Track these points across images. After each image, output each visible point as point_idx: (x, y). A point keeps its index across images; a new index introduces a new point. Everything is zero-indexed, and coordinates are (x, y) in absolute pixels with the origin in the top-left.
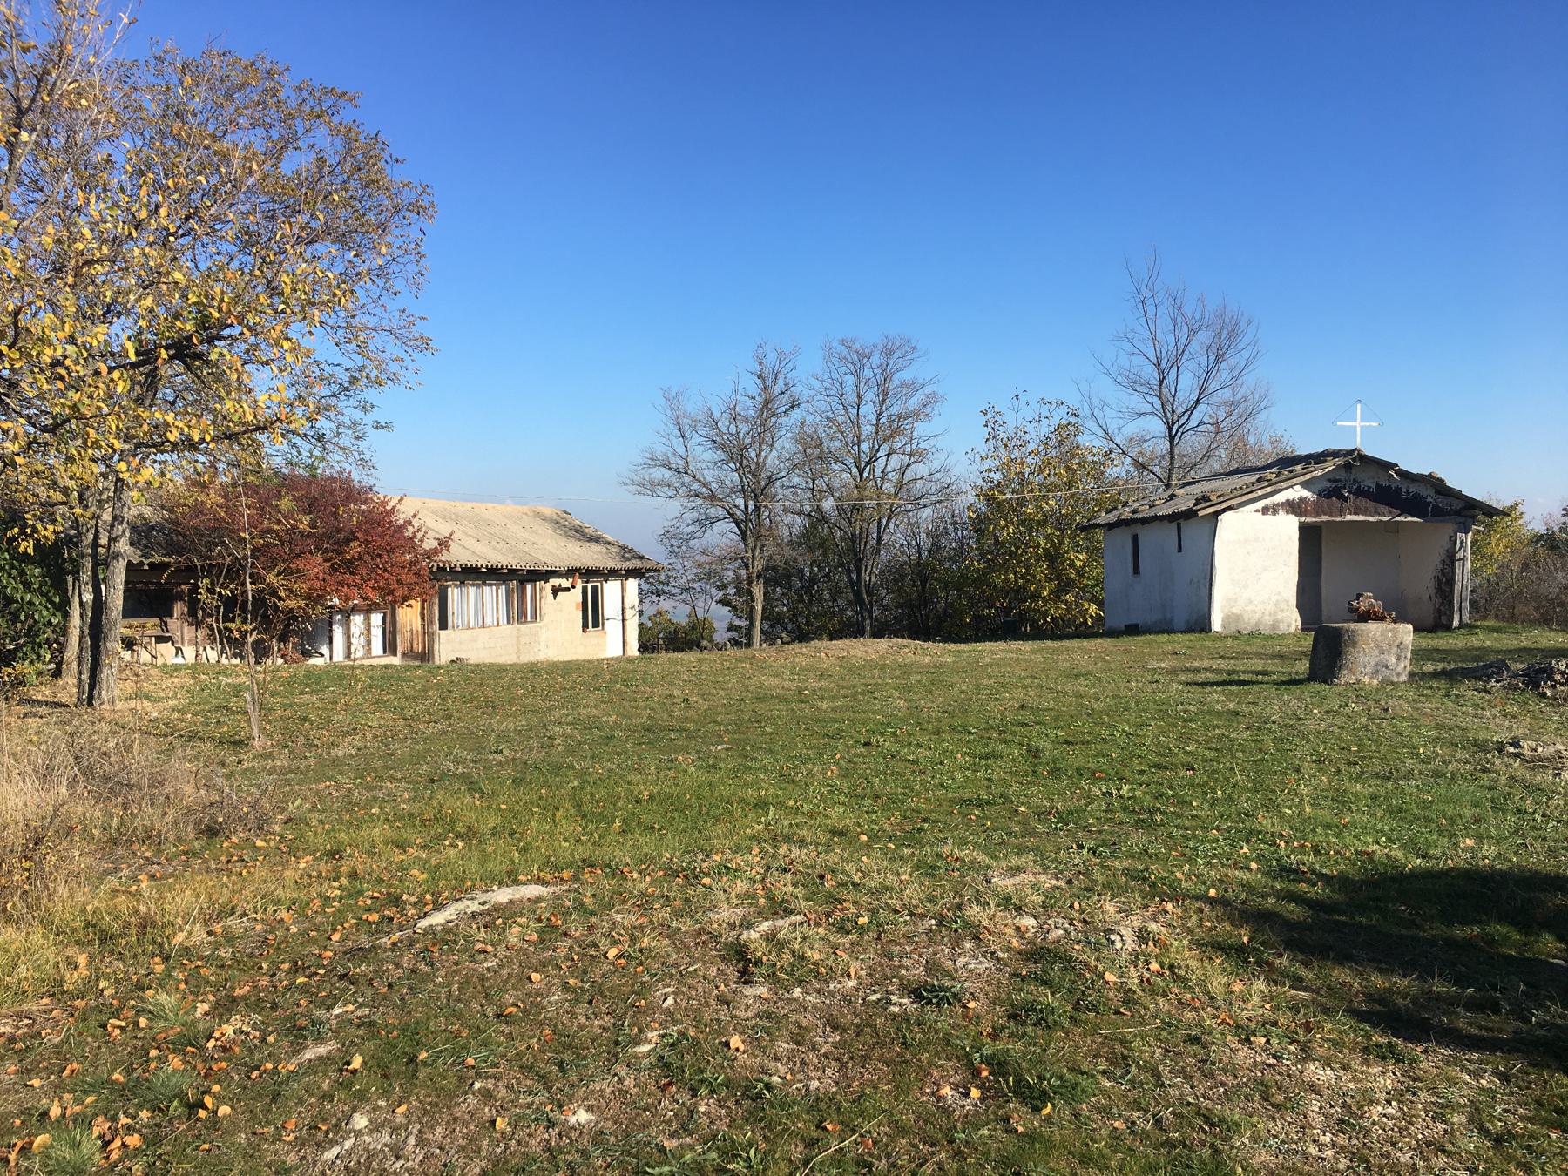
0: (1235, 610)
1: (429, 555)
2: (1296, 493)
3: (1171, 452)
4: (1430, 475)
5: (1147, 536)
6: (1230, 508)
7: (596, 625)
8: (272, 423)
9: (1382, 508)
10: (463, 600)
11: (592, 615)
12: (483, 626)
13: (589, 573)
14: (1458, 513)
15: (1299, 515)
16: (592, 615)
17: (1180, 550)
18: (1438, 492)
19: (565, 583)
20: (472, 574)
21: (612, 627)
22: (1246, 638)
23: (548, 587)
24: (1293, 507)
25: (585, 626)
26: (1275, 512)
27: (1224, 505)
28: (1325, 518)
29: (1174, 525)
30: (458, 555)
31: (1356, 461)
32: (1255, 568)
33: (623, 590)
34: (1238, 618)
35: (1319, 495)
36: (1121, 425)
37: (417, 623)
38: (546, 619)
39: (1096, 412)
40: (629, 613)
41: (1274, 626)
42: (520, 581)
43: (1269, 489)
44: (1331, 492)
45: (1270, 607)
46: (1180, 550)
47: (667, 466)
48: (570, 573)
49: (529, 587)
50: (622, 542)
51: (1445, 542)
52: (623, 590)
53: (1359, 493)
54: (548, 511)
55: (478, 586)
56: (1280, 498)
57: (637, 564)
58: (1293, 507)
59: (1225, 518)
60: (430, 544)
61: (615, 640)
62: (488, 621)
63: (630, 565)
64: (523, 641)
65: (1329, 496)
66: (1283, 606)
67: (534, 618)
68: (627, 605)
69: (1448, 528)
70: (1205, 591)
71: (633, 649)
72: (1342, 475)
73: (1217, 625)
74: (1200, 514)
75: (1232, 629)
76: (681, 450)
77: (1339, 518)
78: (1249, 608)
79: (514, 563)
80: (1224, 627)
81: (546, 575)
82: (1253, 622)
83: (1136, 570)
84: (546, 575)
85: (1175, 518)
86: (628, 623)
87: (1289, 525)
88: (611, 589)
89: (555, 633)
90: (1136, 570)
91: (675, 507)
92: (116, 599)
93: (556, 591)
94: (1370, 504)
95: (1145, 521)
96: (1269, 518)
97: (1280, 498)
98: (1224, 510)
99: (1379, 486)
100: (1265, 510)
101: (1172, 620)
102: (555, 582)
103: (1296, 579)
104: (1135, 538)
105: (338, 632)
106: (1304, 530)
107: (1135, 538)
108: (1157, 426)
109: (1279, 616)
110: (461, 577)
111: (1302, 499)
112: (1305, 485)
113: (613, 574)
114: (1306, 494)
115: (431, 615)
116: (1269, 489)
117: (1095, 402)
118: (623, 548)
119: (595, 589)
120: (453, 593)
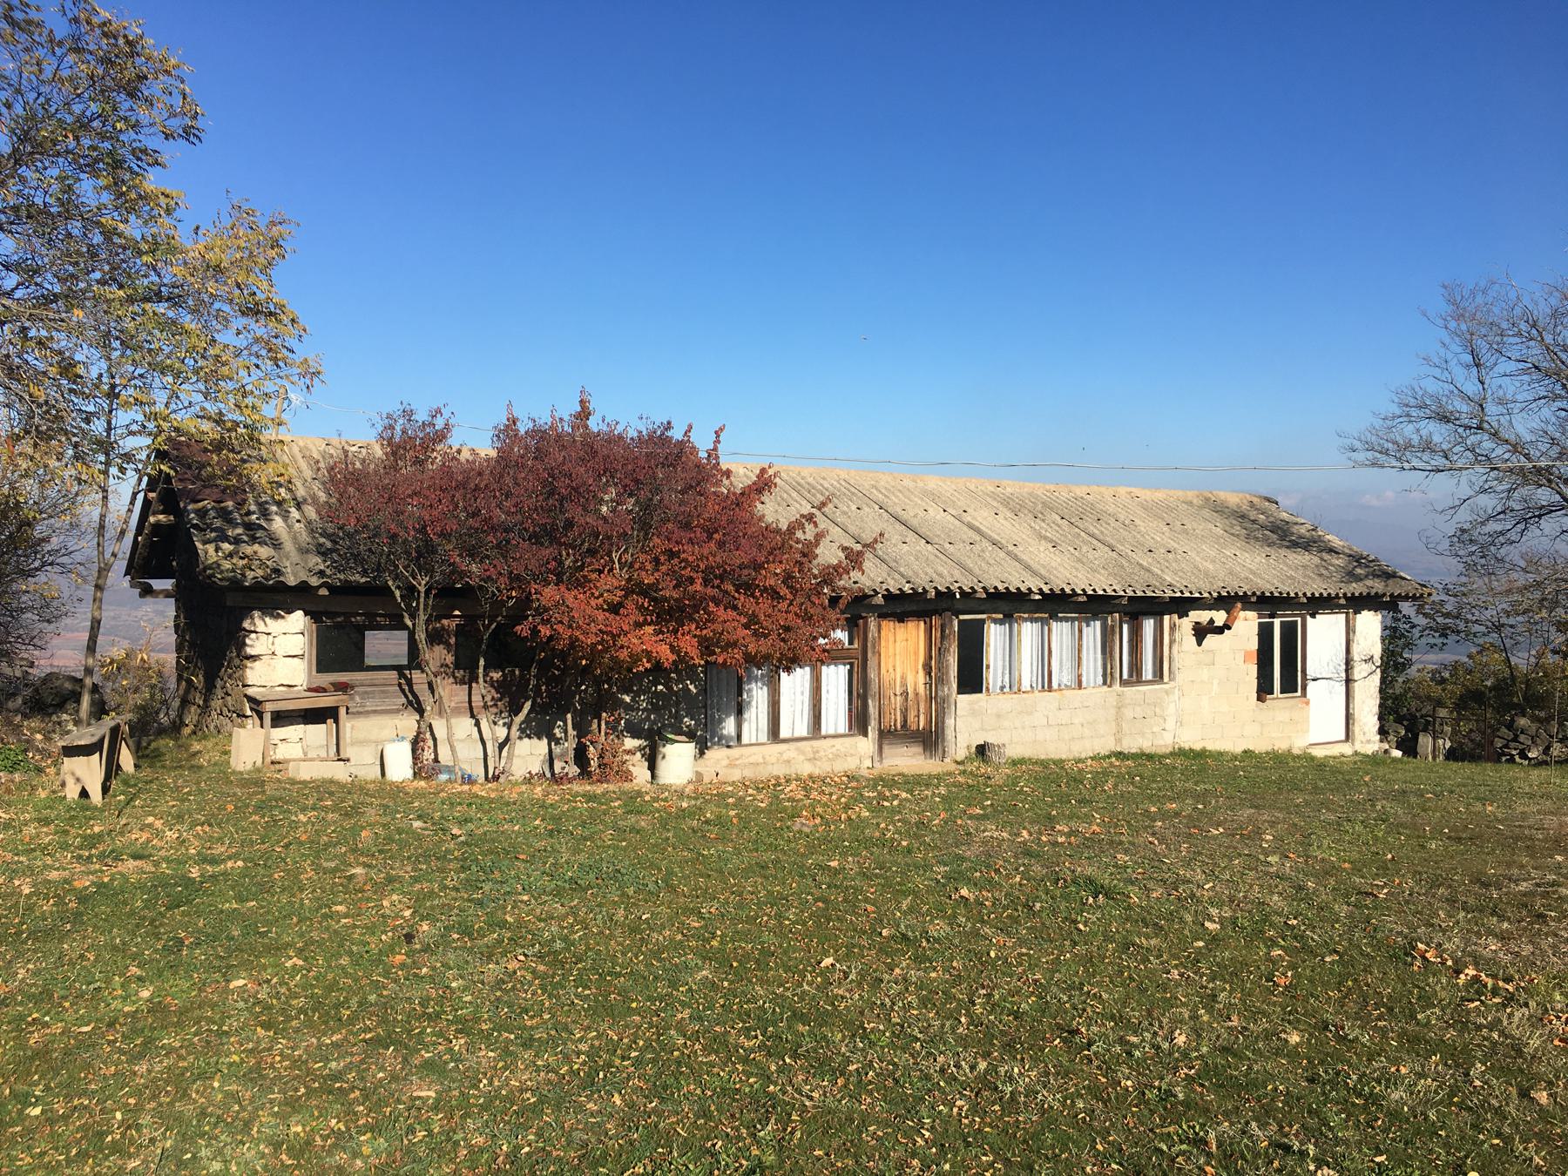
1: (830, 575)
7: (1289, 686)
10: (1010, 647)
11: (1280, 670)
12: (1050, 689)
13: (1266, 603)
16: (1280, 670)
19: (1220, 617)
20: (1011, 604)
21: (1324, 699)
23: (1186, 624)
25: (1264, 689)
30: (872, 577)
33: (1350, 630)
37: (917, 681)
38: (1179, 677)
40: (1360, 670)
42: (1130, 615)
47: (1445, 418)
48: (1225, 601)
49: (1149, 625)
50: (1359, 548)
52: (1350, 630)
54: (1233, 499)
55: (1044, 622)
57: (1378, 586)
60: (828, 554)
61: (1334, 712)
62: (1062, 675)
63: (1357, 588)
64: (1128, 713)
67: (1289, 686)
68: (1356, 656)
71: (1368, 738)
76: (1472, 388)
79: (1102, 583)
81: (1181, 605)
84: (1181, 605)
86: (1357, 687)
88: (1323, 636)
89: (1205, 699)
91: (1444, 488)
92: (421, 636)
93: (1201, 632)
102: (1203, 616)
105: (758, 695)
110: (1005, 607)
113: (1319, 604)
115: (942, 668)
118: (1358, 559)
119: (1289, 632)
120: (995, 635)
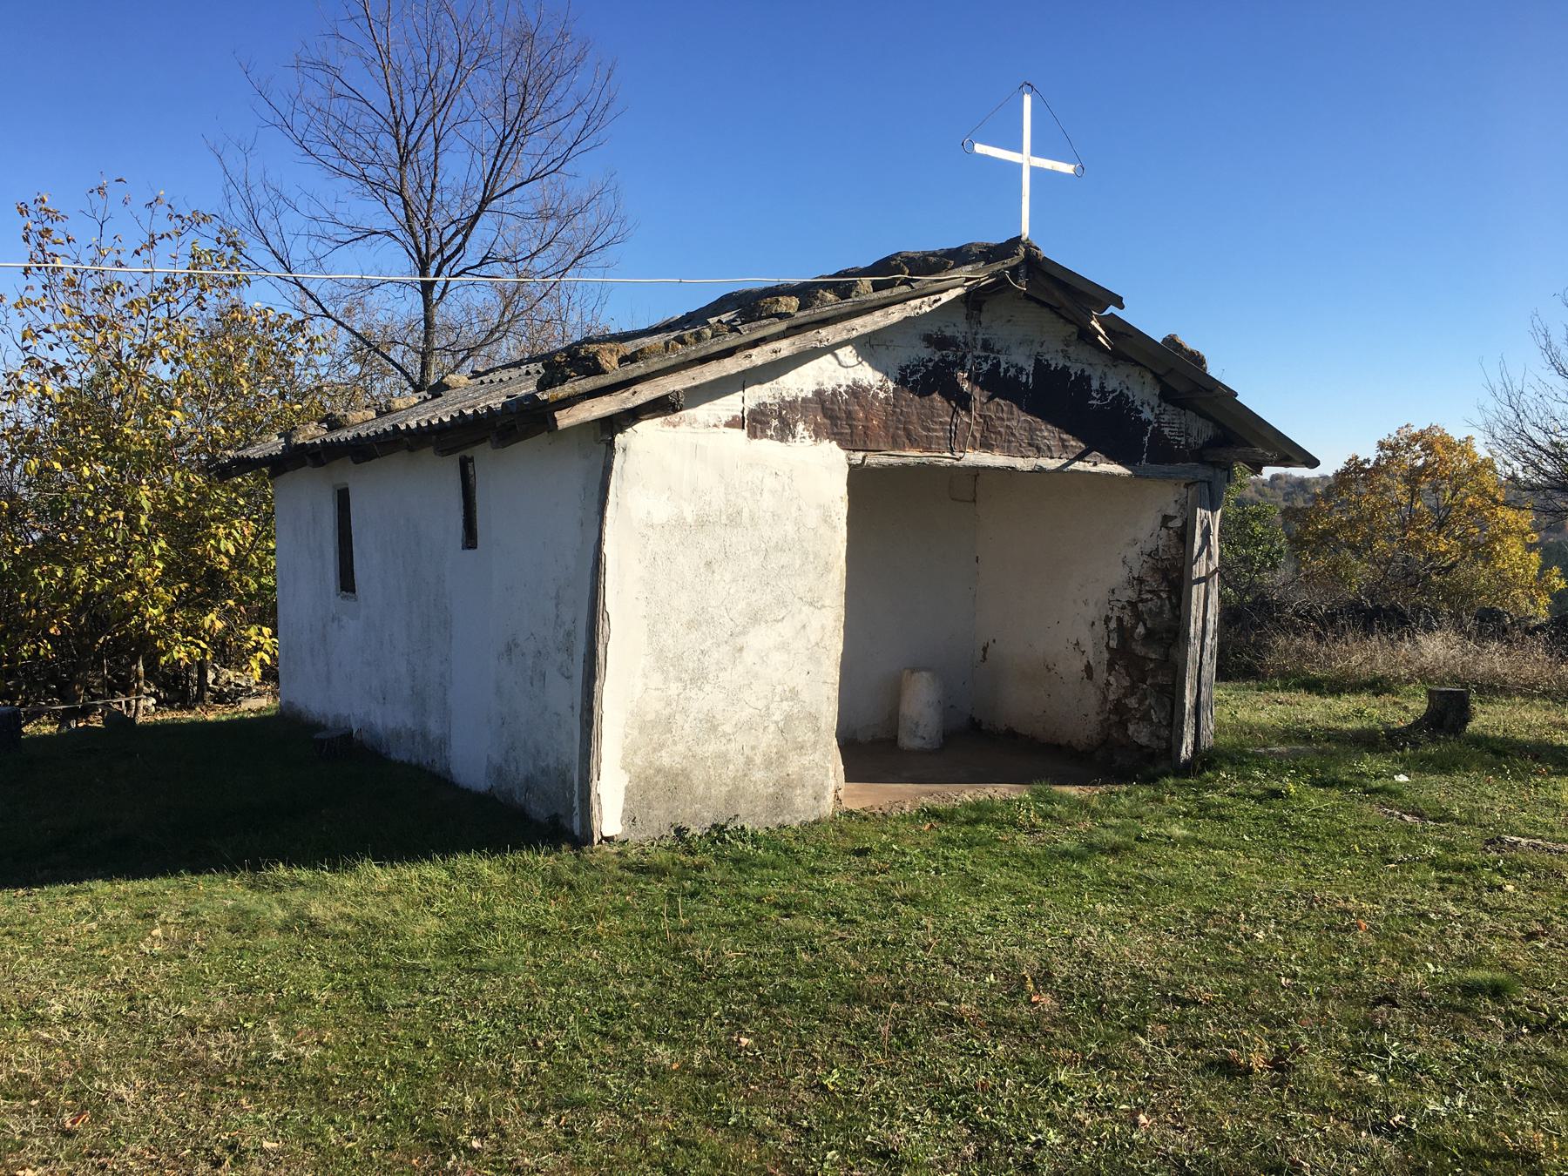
0: (665, 759)
2: (839, 371)
3: (428, 320)
4: (1171, 341)
5: (379, 497)
6: (663, 406)
8: (1331, 618)
9: (1048, 433)
14: (1198, 455)
15: (848, 444)
17: (470, 538)
18: (1168, 396)
22: (709, 857)
24: (834, 416)
26: (785, 432)
27: (645, 393)
28: (913, 456)
29: (451, 465)
31: (1033, 284)
32: (720, 611)
34: (675, 783)
35: (902, 381)
36: (333, 291)
39: (264, 217)
41: (779, 801)
43: (786, 347)
44: (931, 370)
45: (767, 740)
46: (470, 538)
51: (1143, 530)
53: (998, 384)
56: (800, 382)
58: (834, 416)
59: (642, 439)
65: (923, 390)
66: (804, 734)
69: (1165, 497)
70: (563, 695)
72: (958, 328)
73: (609, 818)
74: (565, 419)
75: (659, 822)
77: (946, 459)
78: (712, 747)
80: (631, 819)
82: (719, 792)
83: (347, 582)
85: (462, 438)
87: (819, 471)
90: (347, 582)
94: (1019, 420)
95: (364, 450)
96: (767, 447)
97: (800, 382)
98: (633, 416)
99: (1041, 366)
100: (755, 423)
101: (444, 742)
103: (836, 645)
104: (465, 464)
106: (865, 488)
107: (343, 500)
108: (396, 262)
109: (794, 766)
111: (857, 391)
112: (868, 347)
114: (868, 376)
116: (786, 347)
117: (259, 196)
